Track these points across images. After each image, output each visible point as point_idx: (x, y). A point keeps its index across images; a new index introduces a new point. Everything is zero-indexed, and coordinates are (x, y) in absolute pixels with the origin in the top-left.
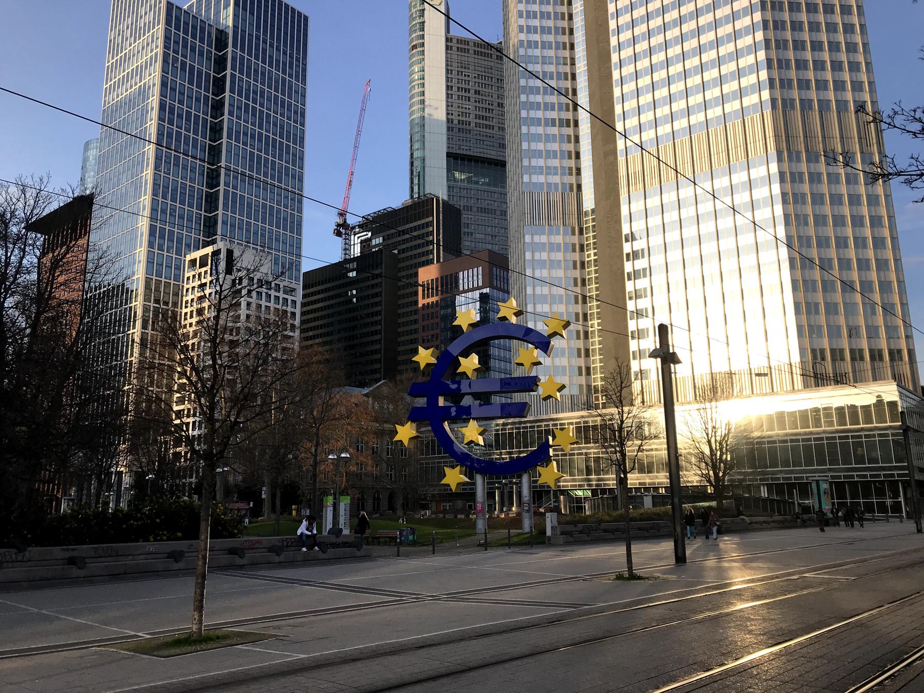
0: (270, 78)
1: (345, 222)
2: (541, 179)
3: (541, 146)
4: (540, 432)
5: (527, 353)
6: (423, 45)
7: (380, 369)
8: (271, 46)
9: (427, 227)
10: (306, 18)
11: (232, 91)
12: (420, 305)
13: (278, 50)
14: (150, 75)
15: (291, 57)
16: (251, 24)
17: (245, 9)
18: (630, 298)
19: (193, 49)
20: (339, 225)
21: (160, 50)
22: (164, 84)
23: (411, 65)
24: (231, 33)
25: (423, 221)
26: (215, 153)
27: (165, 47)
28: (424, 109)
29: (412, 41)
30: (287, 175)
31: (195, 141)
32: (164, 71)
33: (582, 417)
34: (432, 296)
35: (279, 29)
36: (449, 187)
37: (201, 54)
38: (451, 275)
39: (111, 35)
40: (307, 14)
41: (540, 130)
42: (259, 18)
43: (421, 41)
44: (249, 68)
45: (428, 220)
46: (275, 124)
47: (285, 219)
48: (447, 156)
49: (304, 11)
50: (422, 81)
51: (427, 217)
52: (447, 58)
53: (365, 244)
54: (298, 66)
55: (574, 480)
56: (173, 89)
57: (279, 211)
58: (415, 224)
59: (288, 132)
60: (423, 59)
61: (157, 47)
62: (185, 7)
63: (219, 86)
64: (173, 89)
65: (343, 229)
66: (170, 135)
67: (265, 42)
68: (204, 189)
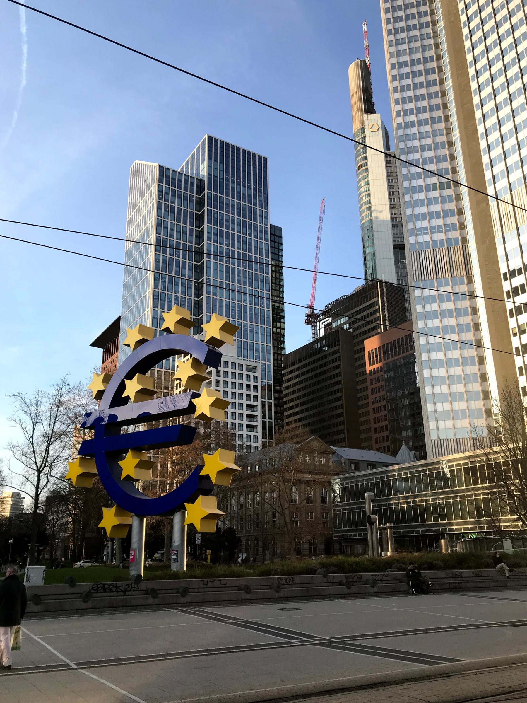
0: (239, 208)
1: (313, 312)
2: (427, 238)
3: (424, 210)
4: (431, 476)
6: (366, 164)
7: (344, 429)
8: (238, 184)
9: (374, 306)
10: (265, 160)
11: (209, 222)
12: (368, 372)
13: (244, 186)
14: (150, 220)
15: (255, 190)
16: (222, 171)
17: (216, 160)
18: (515, 335)
19: (179, 197)
20: (308, 316)
21: (155, 202)
22: (158, 225)
23: (359, 181)
24: (206, 179)
25: (370, 302)
26: (199, 270)
27: (159, 198)
28: (371, 214)
29: (358, 163)
30: (256, 280)
31: (184, 263)
32: (159, 215)
33: (469, 457)
34: (377, 363)
35: (244, 171)
36: (398, 273)
37: (186, 199)
38: (391, 342)
39: (129, 199)
40: (265, 156)
41: (422, 196)
42: (227, 165)
43: (365, 161)
44: (221, 203)
45: (374, 300)
46: (245, 243)
47: (257, 315)
48: (394, 248)
49: (263, 155)
50: (368, 193)
51: (374, 298)
52: (387, 170)
53: (328, 326)
54: (260, 196)
55: (466, 523)
56: (166, 228)
57: (251, 309)
58: (361, 307)
59: (261, 249)
60: (368, 175)
61: (153, 199)
62: (179, 170)
63: (200, 219)
64: (166, 228)
65: (312, 319)
66: (164, 262)
67: (233, 182)
68: (193, 298)
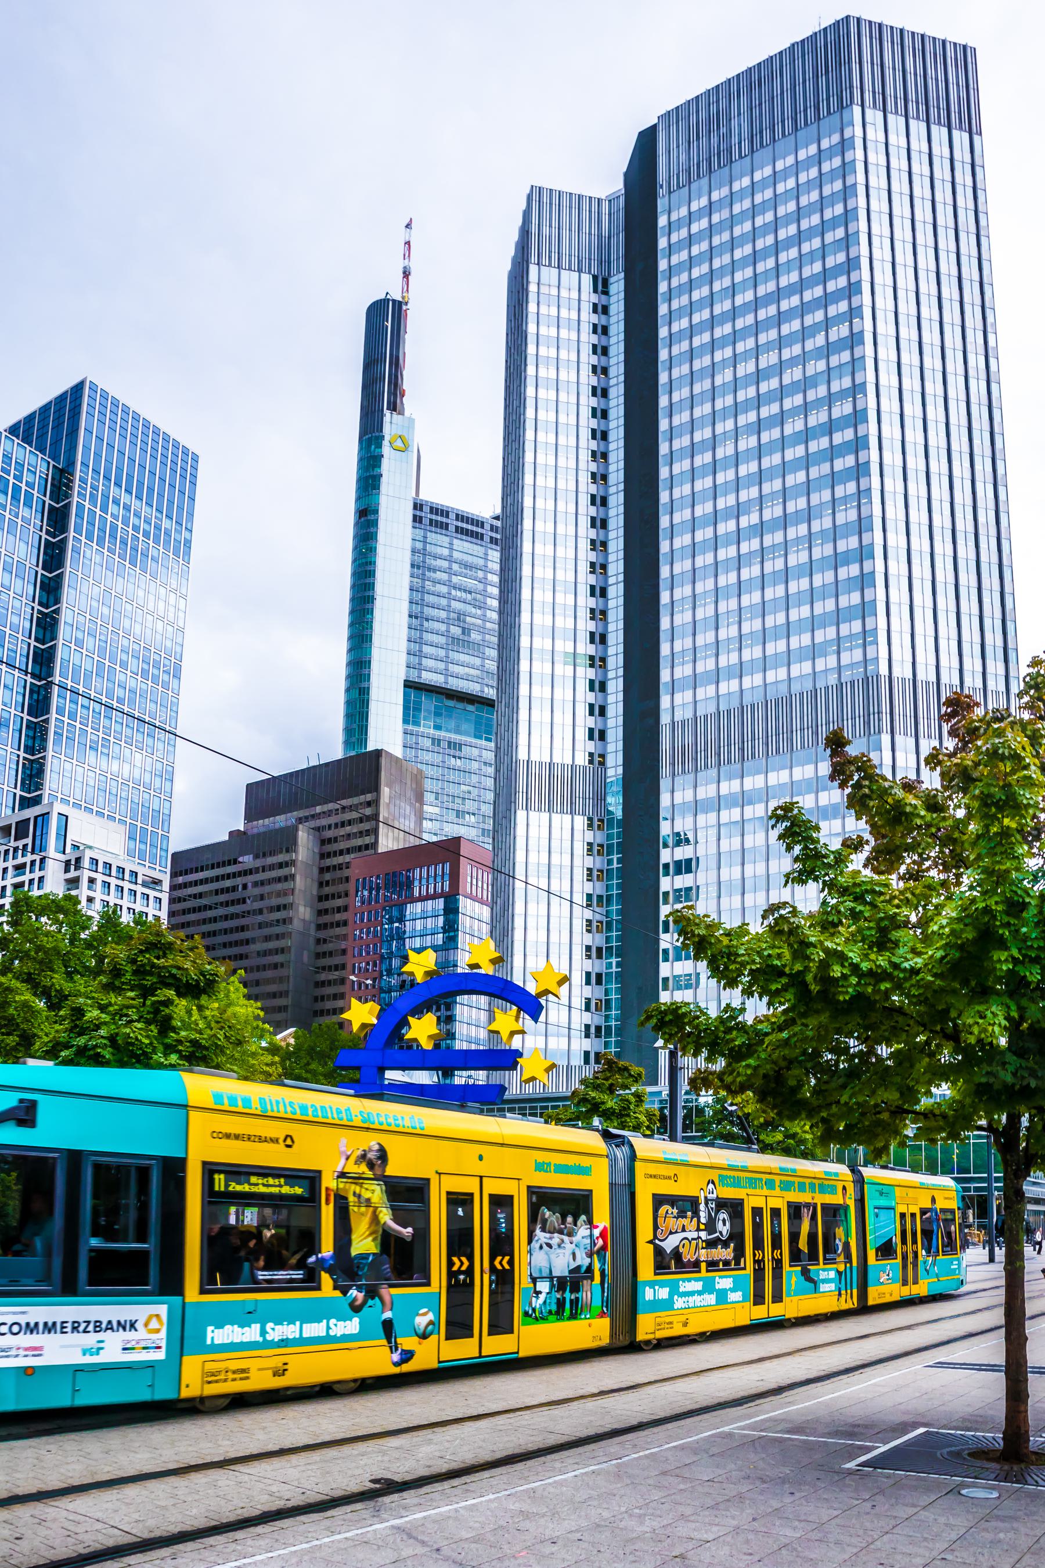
5: (506, 1020)
